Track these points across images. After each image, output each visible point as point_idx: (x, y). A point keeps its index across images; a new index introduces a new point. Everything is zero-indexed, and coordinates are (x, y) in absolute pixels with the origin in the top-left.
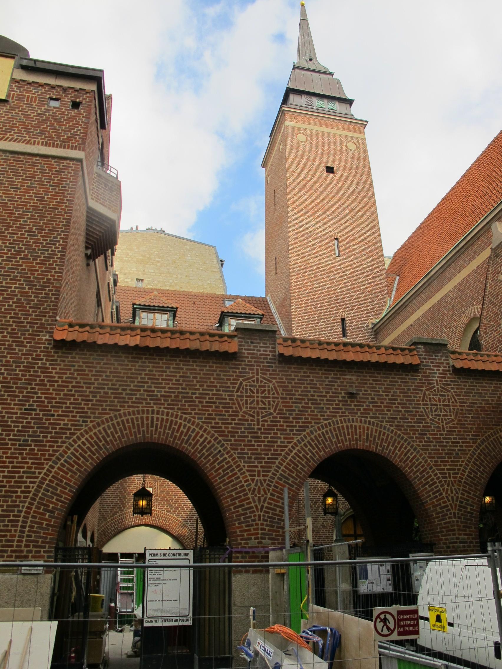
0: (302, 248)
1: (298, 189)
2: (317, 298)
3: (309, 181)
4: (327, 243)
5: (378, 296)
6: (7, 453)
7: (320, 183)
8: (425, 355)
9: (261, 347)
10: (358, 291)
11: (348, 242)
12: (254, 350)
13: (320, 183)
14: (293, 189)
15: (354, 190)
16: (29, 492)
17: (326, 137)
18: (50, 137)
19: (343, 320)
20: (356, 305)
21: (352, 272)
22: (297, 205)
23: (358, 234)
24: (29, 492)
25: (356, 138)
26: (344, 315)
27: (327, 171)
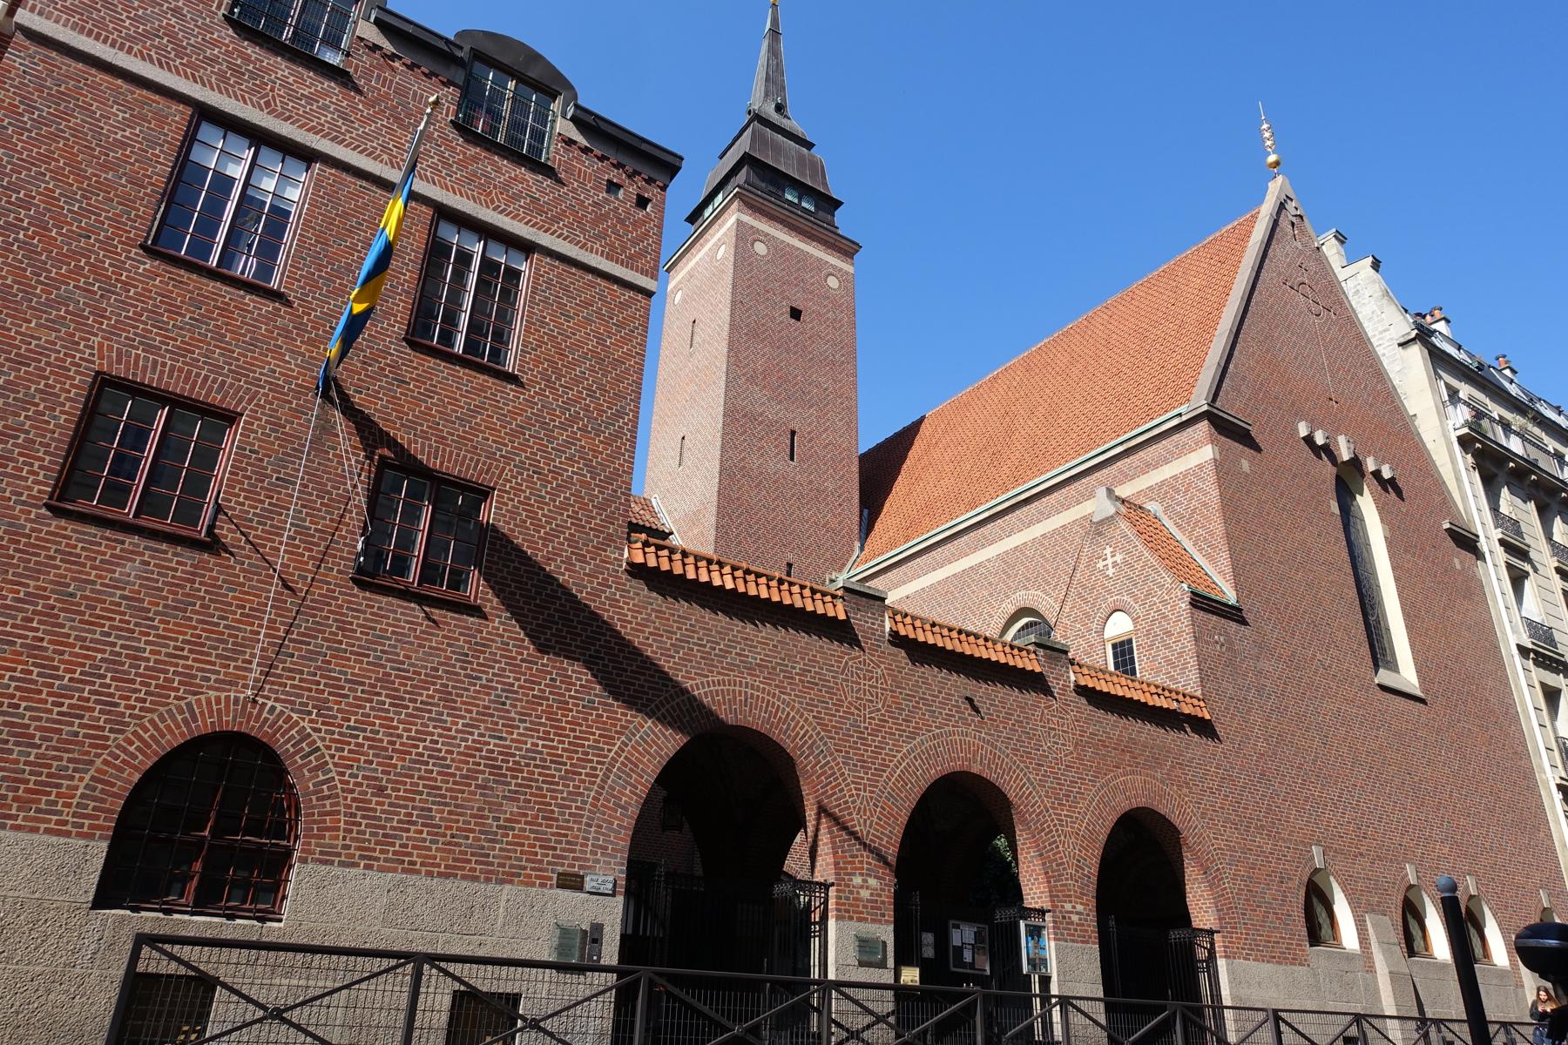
6: (62, 705)
16: (596, 776)
18: (612, 245)
24: (596, 776)
26: (790, 557)
27: (800, 312)
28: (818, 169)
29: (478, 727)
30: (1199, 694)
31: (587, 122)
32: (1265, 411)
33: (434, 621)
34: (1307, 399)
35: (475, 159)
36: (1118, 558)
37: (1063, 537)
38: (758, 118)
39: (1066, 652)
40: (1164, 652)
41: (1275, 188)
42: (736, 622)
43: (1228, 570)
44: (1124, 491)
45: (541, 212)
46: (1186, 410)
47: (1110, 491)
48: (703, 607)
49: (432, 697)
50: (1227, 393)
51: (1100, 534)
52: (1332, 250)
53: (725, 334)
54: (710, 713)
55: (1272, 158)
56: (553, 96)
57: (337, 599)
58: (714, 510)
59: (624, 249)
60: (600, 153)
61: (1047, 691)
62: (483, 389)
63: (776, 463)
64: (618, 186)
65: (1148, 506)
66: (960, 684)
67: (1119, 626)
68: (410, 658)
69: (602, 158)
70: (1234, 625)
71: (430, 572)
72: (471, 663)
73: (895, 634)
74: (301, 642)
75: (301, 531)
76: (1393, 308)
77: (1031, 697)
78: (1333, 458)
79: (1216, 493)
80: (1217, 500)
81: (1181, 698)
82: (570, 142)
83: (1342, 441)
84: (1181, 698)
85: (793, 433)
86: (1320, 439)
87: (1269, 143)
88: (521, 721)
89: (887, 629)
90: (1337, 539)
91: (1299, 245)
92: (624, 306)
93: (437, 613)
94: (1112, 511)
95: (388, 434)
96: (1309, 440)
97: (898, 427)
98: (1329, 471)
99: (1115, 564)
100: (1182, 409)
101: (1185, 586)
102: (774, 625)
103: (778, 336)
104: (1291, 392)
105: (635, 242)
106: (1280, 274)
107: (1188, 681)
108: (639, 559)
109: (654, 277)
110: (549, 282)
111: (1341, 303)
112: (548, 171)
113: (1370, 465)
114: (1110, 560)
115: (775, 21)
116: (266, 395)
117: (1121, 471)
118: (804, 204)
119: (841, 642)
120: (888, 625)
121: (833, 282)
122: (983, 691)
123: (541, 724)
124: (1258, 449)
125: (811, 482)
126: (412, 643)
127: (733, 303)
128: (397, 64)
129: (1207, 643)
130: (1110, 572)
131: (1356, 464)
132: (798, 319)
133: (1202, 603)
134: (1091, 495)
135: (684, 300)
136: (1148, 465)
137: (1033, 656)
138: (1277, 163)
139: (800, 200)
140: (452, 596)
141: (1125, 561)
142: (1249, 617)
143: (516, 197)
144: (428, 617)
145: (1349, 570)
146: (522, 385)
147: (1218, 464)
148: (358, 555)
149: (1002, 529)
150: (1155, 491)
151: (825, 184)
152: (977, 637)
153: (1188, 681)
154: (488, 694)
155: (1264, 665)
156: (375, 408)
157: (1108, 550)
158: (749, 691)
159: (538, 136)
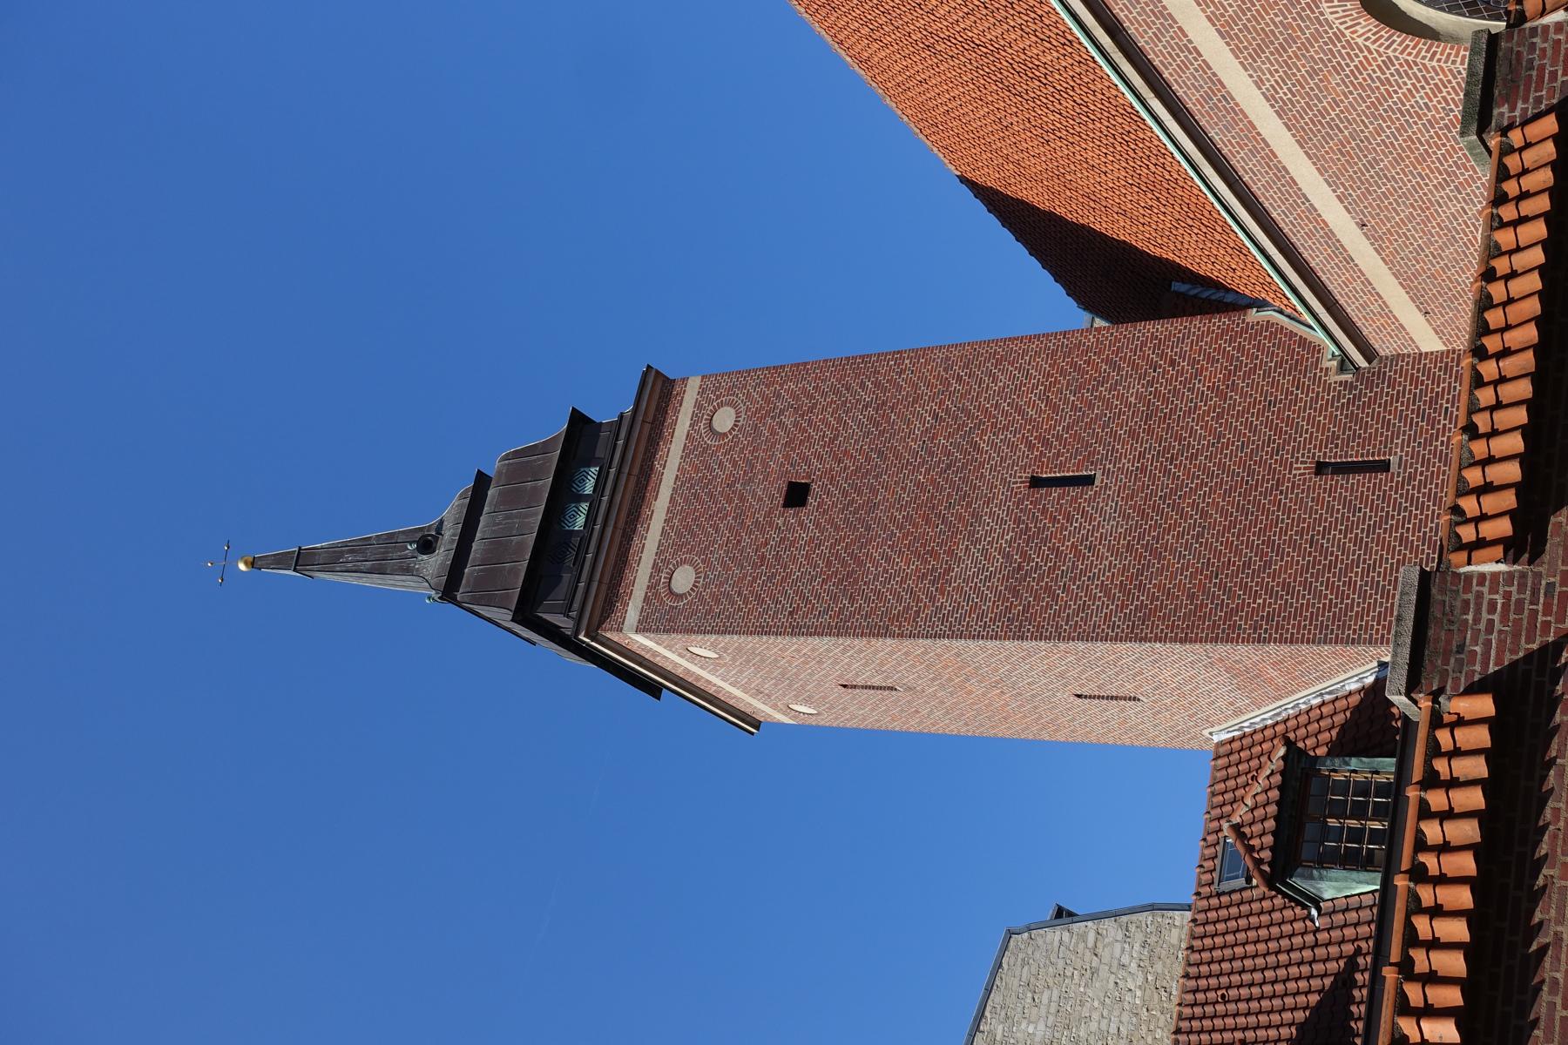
0: (1055, 598)
1: (852, 600)
2: (1238, 552)
3: (829, 564)
4: (1044, 511)
5: (1241, 349)
7: (837, 528)
8: (1526, 100)
9: (1477, 620)
10: (1220, 416)
11: (1047, 443)
12: (1488, 643)
13: (837, 528)
14: (852, 615)
15: (870, 419)
17: (686, 500)
19: (1320, 468)
20: (1269, 424)
21: (1150, 432)
22: (908, 608)
23: (1019, 410)
25: (698, 406)
26: (1302, 468)
38: (449, 591)
39: (1493, 39)
42: (1541, 1009)
53: (859, 643)
58: (1223, 649)
63: (1104, 514)
73: (1513, 548)
85: (1036, 482)
89: (1502, 567)
97: (993, 221)
102: (1536, 896)
115: (280, 561)
118: (589, 488)
120: (1489, 565)
121: (724, 420)
125: (1133, 434)
127: (796, 631)
135: (807, 701)
137: (1516, 137)
139: (581, 498)
149: (1183, 67)
151: (544, 448)
152: (1485, 303)
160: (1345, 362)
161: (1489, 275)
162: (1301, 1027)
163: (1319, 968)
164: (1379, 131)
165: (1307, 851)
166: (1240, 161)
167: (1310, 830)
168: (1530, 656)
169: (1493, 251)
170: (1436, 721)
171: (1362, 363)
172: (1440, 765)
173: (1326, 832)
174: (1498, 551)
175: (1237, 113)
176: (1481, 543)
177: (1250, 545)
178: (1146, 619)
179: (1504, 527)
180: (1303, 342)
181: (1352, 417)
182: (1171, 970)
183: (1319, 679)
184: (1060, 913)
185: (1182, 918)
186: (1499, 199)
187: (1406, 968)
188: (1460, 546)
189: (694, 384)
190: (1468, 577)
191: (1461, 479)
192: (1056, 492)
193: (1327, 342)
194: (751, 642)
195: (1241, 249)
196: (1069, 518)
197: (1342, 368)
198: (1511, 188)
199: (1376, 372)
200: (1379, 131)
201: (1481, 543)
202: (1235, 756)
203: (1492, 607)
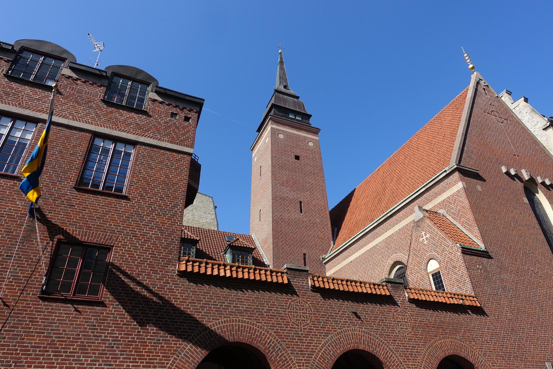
11: (308, 204)
18: (173, 138)
19: (305, 254)
20: (313, 245)
25: (313, 139)
26: (305, 251)
28: (302, 105)
29: (98, 361)
30: (473, 294)
31: (163, 93)
32: (485, 164)
33: (79, 312)
34: (504, 157)
35: (111, 112)
36: (428, 236)
37: (408, 229)
38: (277, 91)
40: (454, 276)
41: (474, 77)
42: (233, 291)
43: (479, 235)
44: (428, 207)
45: (140, 129)
46: (448, 169)
47: (420, 208)
48: (216, 286)
49: (76, 349)
50: (465, 159)
51: (419, 226)
52: (506, 98)
53: (270, 169)
54: (221, 337)
55: (471, 66)
56: (148, 85)
57: (30, 307)
58: (271, 236)
59: (178, 138)
60: (167, 103)
61: (395, 303)
62: (110, 203)
63: (295, 215)
64: (176, 114)
65: (440, 211)
66: (349, 306)
67: (433, 266)
68: (65, 331)
69: (169, 105)
70: (486, 259)
71: (80, 289)
72: (97, 329)
73: (314, 287)
74: (10, 331)
75: (16, 278)
76: (537, 115)
77: (386, 308)
78: (521, 179)
79: (467, 202)
80: (468, 205)
81: (464, 297)
82: (154, 101)
83: (523, 171)
84: (464, 297)
85: (301, 202)
86: (513, 172)
87: (468, 61)
88: (121, 355)
89: (310, 285)
90: (530, 214)
91: (489, 97)
92: (179, 160)
93: (80, 308)
94: (422, 216)
95: (63, 229)
96: (508, 173)
98: (520, 185)
99: (427, 239)
100: (446, 169)
101: (458, 245)
102: (253, 290)
103: (291, 168)
104: (495, 155)
105: (183, 135)
106: (482, 109)
107: (467, 289)
108: (183, 268)
109: (192, 147)
110: (144, 156)
111: (512, 116)
112: (145, 113)
113: (539, 180)
114: (425, 237)
115: (281, 58)
116: (6, 220)
117: (426, 199)
118: (297, 118)
119: (287, 294)
121: (311, 144)
122: (360, 308)
123: (132, 355)
124: (484, 180)
125: (310, 220)
126: (67, 324)
127: (272, 157)
128: (79, 82)
129: (473, 270)
130: (426, 242)
131: (532, 180)
132: (299, 159)
133: (467, 251)
134: (413, 211)
135: (257, 160)
136: (437, 194)
137: (385, 288)
138: (473, 68)
139: (295, 117)
140: (92, 298)
141: (431, 237)
142: (492, 255)
143: (129, 124)
144: (76, 310)
145: (539, 227)
146: (129, 200)
147: (466, 189)
148: (43, 286)
150: (443, 204)
151: (305, 110)
152: (356, 282)
153: (467, 289)
154: (105, 344)
155: (505, 276)
156: (56, 219)
157: (423, 233)
158: (240, 324)
159: (141, 100)
160: (324, 259)
161: (361, 283)
162: (202, 251)
163: (213, 254)
164: (370, 265)
165: (235, 252)
166: (364, 239)
167: (239, 252)
168: (295, 290)
169: (365, 283)
170: (282, 273)
171: (324, 262)
172: (274, 274)
173: (238, 255)
174: (313, 284)
175: (374, 239)
176: (314, 281)
177: (290, 242)
178: (277, 223)
179: (317, 285)
180: (327, 251)
181: (314, 260)
182: (206, 227)
183: (266, 254)
184: (216, 207)
185: (216, 229)
186: (374, 285)
187: (238, 267)
188: (313, 277)
189: (318, 138)
190: (308, 279)
191: (325, 278)
192: (299, 206)
193: (328, 256)
194: (270, 149)
195: (345, 240)
196: (294, 208)
197: (323, 258)
198: (376, 287)
199: (323, 264)
200: (370, 265)
201: (314, 281)
202: (249, 239)
203: (303, 283)
